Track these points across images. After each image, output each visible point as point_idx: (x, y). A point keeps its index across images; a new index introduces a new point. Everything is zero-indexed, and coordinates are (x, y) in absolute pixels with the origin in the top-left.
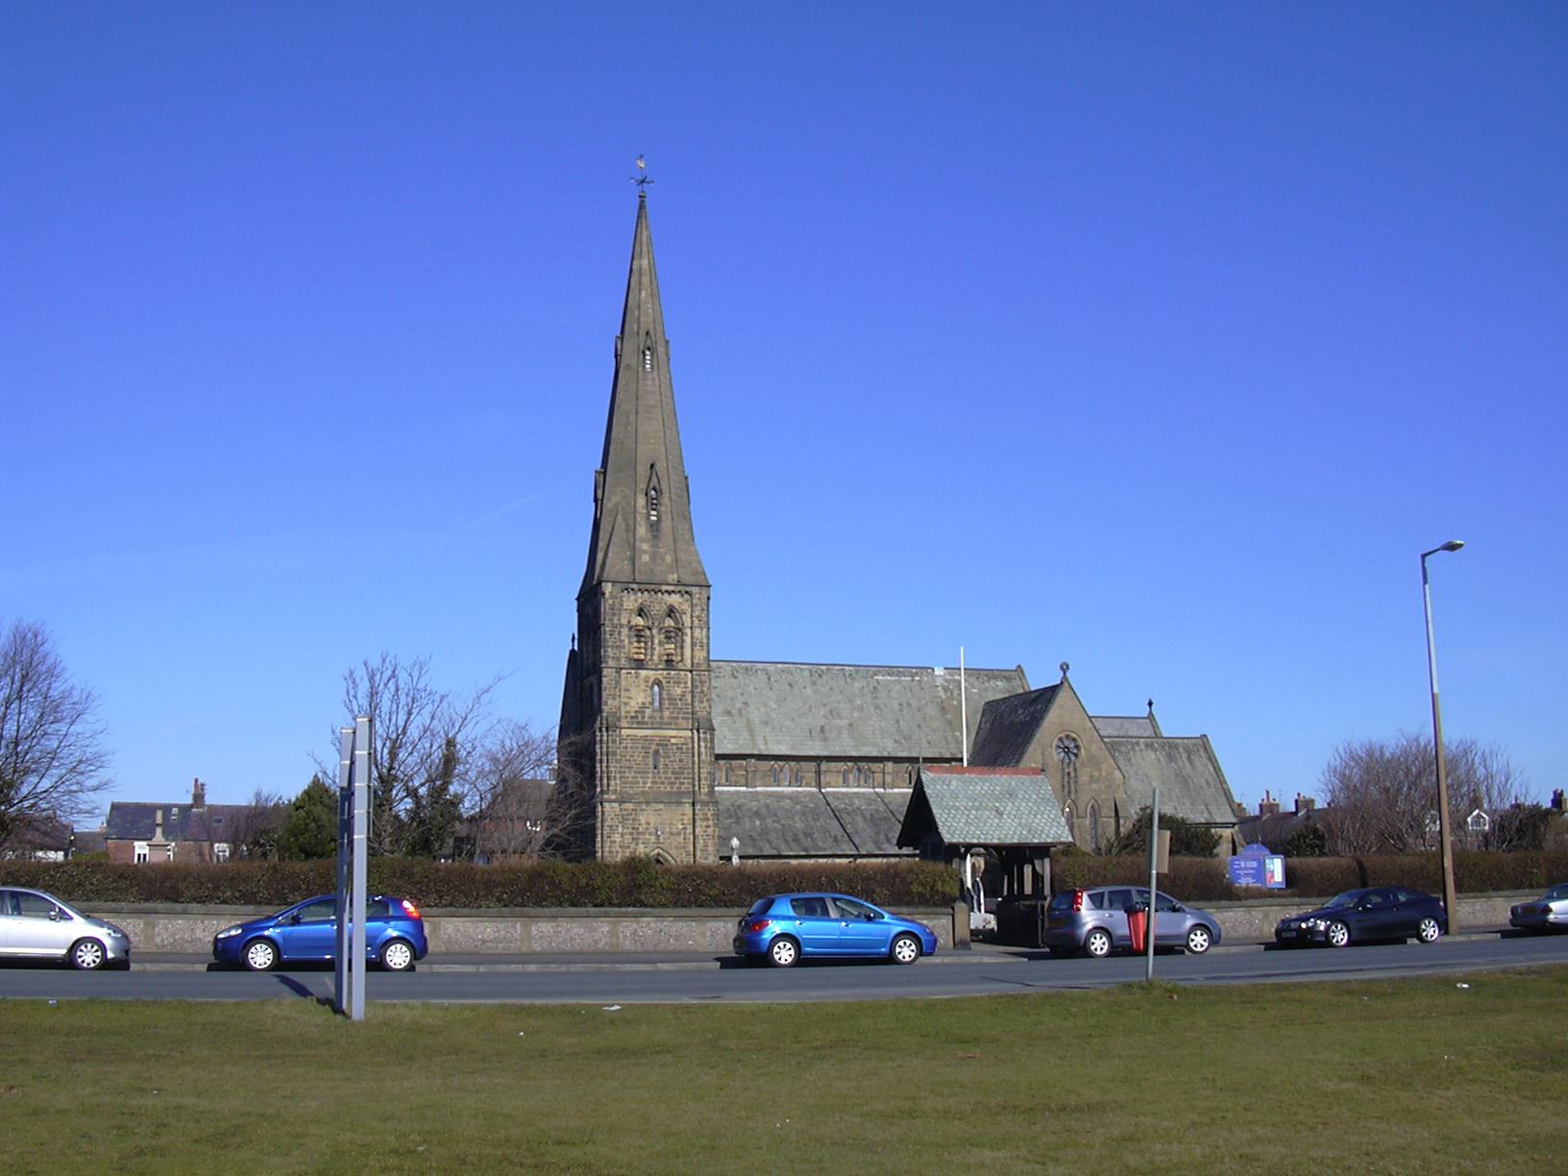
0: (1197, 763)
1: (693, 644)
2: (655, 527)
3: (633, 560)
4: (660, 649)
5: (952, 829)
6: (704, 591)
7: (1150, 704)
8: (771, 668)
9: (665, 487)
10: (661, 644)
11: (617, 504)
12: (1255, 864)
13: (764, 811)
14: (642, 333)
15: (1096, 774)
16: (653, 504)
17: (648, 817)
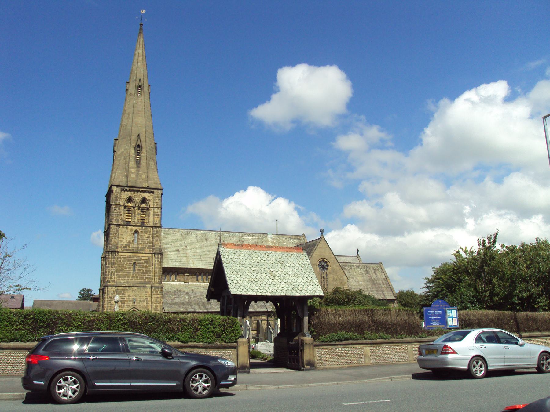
0: (378, 274)
1: (154, 215)
2: (138, 163)
3: (127, 176)
4: (137, 217)
5: (237, 286)
6: (160, 192)
7: (358, 251)
8: (198, 232)
9: (144, 145)
10: (139, 214)
11: (122, 152)
12: (440, 313)
13: (190, 293)
14: (138, 80)
15: (336, 277)
16: (138, 153)
17: (130, 293)
